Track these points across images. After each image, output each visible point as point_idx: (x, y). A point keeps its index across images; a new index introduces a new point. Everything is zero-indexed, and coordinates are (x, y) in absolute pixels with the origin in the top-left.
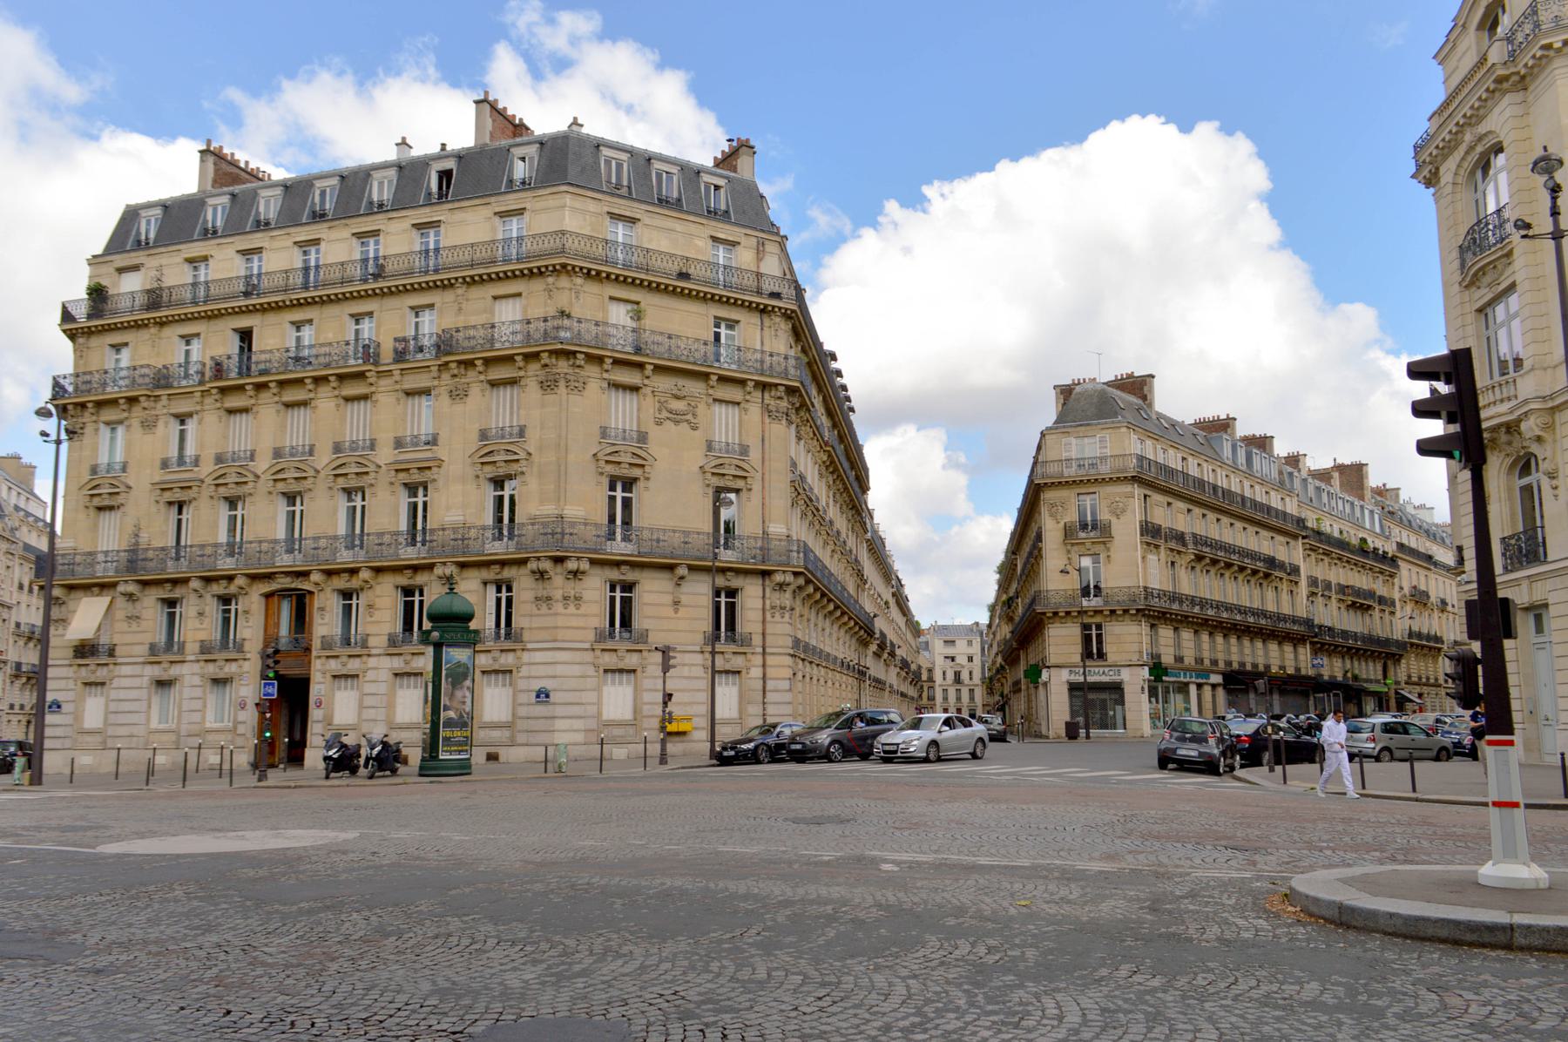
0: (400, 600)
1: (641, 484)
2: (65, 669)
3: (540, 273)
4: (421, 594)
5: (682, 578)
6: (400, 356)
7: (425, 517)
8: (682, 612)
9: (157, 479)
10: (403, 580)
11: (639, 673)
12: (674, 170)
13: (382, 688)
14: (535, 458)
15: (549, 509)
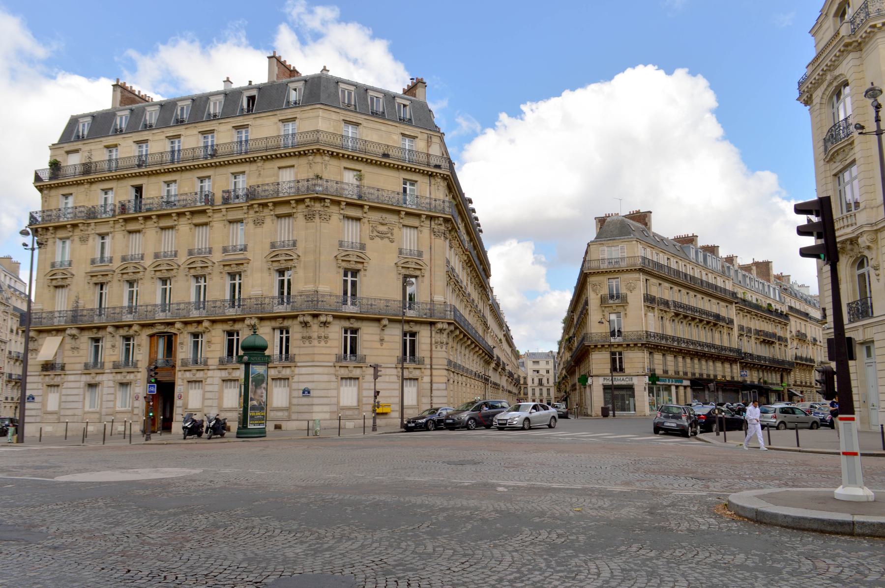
0: (226, 338)
2: (37, 378)
3: (305, 154)
4: (238, 335)
5: (385, 326)
6: (226, 201)
7: (240, 292)
9: (89, 270)
10: (227, 327)
12: (381, 96)
14: (302, 258)
15: (310, 287)
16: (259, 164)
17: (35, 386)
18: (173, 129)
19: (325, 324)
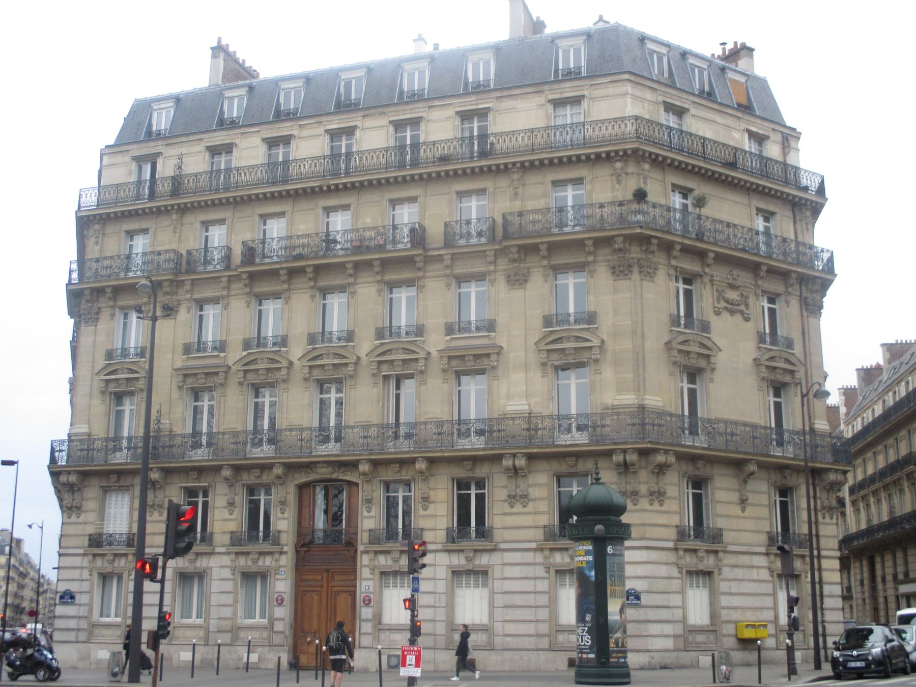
1: (707, 375)
2: (79, 559)
3: (609, 158)
6: (449, 241)
8: (749, 509)
9: (179, 364)
10: (461, 473)
11: (716, 575)
12: (704, 66)
13: (441, 587)
14: (610, 345)
15: (629, 399)
16: (515, 176)
17: (640, 570)
18: (144, 145)
19: (515, 472)
